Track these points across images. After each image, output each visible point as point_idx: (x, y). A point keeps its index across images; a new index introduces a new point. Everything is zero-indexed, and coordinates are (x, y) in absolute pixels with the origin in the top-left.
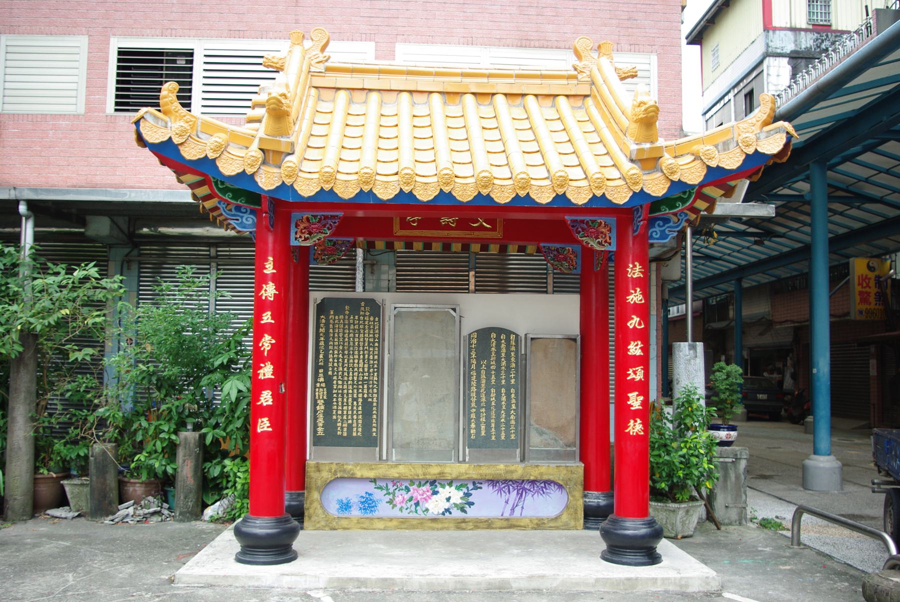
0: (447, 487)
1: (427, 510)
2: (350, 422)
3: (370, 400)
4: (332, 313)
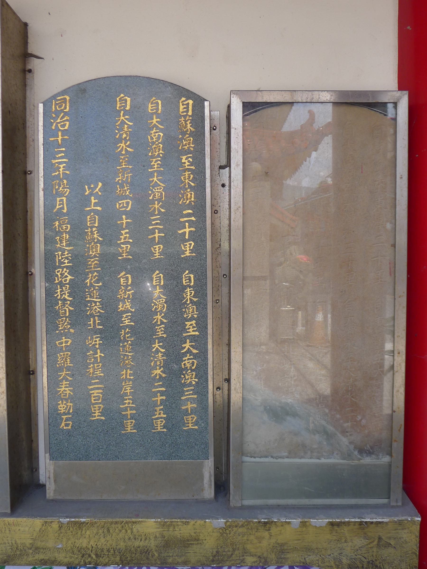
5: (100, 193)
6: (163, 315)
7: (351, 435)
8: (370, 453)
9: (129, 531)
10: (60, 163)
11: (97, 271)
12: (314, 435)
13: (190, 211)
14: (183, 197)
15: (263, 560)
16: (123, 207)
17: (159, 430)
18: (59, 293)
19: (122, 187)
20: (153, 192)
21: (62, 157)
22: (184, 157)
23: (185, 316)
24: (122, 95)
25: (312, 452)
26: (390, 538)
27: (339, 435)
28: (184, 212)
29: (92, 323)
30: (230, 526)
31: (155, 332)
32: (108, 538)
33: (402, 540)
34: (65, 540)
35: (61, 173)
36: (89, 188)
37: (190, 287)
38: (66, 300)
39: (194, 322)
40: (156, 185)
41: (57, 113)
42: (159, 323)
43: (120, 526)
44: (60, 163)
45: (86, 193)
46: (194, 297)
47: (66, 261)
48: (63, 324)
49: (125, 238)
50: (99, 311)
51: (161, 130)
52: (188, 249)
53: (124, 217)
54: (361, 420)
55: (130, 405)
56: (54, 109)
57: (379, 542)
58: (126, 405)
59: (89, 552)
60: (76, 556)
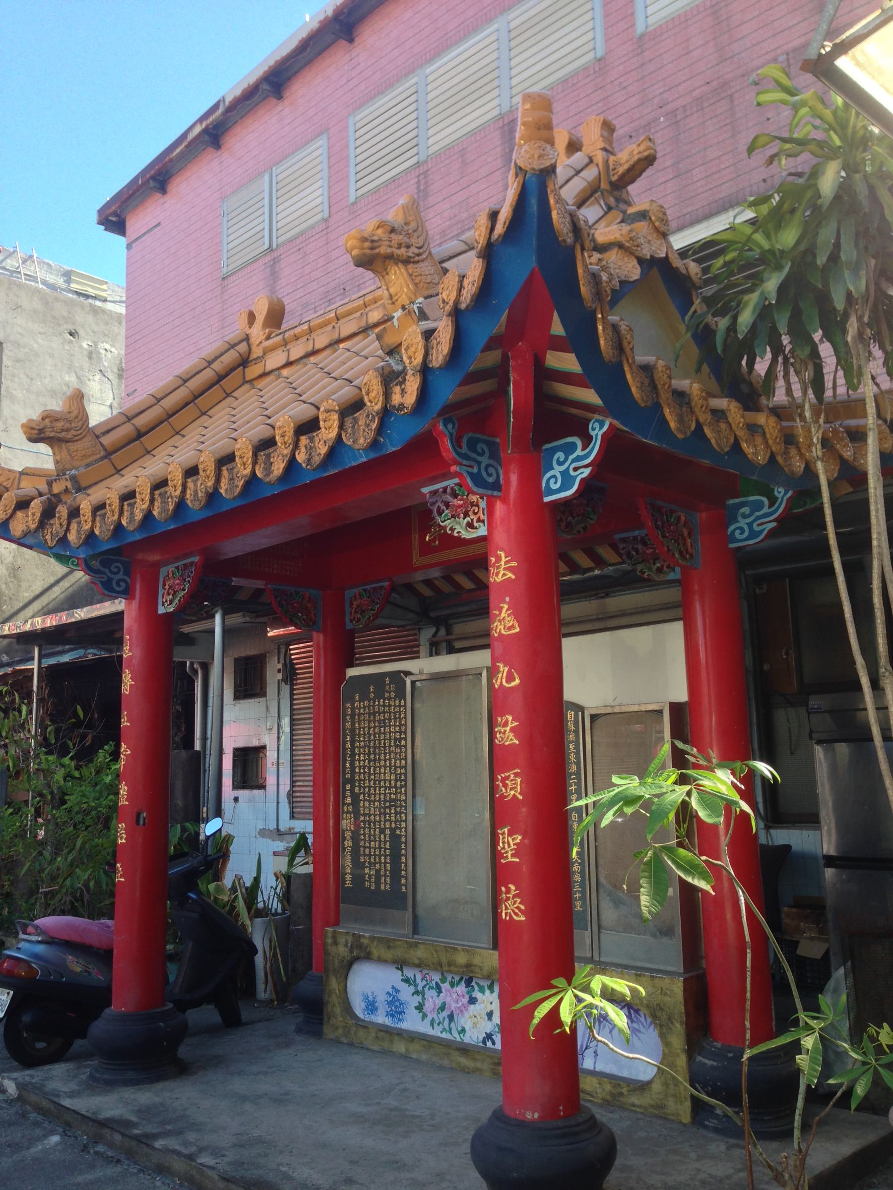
0: (487, 992)
1: (463, 1031)
2: (378, 867)
3: (398, 832)
4: (357, 698)
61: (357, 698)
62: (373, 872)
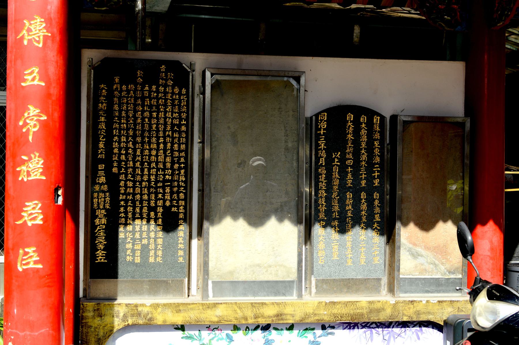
2: (145, 242)
3: (174, 209)
4: (117, 80)
5: (339, 157)
6: (365, 211)
7: (445, 265)
8: (453, 273)
9: (355, 306)
10: (322, 143)
11: (337, 192)
12: (430, 265)
13: (378, 166)
14: (375, 159)
15: (411, 318)
16: (349, 163)
17: (362, 264)
18: (320, 201)
19: (349, 154)
20: (362, 157)
21: (323, 140)
22: (376, 142)
23: (375, 212)
24: (350, 114)
25: (429, 273)
26: (463, 308)
27: (440, 265)
28: (375, 166)
29: (334, 215)
30: (397, 303)
31: (361, 219)
32: (346, 309)
33: (468, 309)
34: (327, 310)
35: (322, 147)
36: (335, 155)
37: (377, 199)
38: (323, 204)
39: (378, 215)
40: (363, 154)
41: (321, 120)
42: (363, 215)
43: (351, 303)
44: (322, 143)
45: (333, 157)
46: (378, 204)
47: (324, 187)
48: (322, 215)
49: (350, 177)
50: (337, 210)
51: (366, 130)
52: (376, 182)
53: (349, 168)
54: (449, 258)
55: (350, 253)
56: (89, 4)
57: (458, 309)
58: (349, 252)
59: (338, 315)
60: (332, 317)
61: (117, 80)
62: (138, 247)
